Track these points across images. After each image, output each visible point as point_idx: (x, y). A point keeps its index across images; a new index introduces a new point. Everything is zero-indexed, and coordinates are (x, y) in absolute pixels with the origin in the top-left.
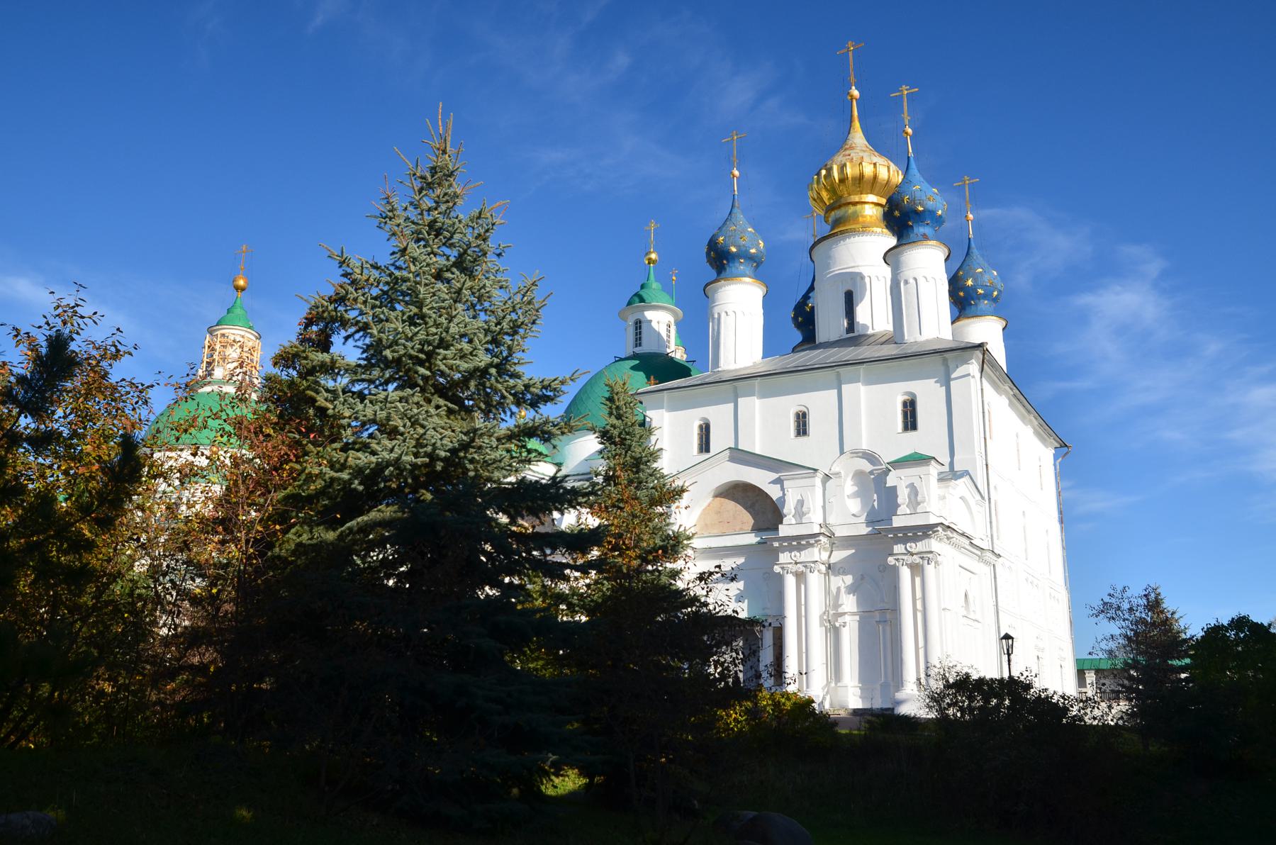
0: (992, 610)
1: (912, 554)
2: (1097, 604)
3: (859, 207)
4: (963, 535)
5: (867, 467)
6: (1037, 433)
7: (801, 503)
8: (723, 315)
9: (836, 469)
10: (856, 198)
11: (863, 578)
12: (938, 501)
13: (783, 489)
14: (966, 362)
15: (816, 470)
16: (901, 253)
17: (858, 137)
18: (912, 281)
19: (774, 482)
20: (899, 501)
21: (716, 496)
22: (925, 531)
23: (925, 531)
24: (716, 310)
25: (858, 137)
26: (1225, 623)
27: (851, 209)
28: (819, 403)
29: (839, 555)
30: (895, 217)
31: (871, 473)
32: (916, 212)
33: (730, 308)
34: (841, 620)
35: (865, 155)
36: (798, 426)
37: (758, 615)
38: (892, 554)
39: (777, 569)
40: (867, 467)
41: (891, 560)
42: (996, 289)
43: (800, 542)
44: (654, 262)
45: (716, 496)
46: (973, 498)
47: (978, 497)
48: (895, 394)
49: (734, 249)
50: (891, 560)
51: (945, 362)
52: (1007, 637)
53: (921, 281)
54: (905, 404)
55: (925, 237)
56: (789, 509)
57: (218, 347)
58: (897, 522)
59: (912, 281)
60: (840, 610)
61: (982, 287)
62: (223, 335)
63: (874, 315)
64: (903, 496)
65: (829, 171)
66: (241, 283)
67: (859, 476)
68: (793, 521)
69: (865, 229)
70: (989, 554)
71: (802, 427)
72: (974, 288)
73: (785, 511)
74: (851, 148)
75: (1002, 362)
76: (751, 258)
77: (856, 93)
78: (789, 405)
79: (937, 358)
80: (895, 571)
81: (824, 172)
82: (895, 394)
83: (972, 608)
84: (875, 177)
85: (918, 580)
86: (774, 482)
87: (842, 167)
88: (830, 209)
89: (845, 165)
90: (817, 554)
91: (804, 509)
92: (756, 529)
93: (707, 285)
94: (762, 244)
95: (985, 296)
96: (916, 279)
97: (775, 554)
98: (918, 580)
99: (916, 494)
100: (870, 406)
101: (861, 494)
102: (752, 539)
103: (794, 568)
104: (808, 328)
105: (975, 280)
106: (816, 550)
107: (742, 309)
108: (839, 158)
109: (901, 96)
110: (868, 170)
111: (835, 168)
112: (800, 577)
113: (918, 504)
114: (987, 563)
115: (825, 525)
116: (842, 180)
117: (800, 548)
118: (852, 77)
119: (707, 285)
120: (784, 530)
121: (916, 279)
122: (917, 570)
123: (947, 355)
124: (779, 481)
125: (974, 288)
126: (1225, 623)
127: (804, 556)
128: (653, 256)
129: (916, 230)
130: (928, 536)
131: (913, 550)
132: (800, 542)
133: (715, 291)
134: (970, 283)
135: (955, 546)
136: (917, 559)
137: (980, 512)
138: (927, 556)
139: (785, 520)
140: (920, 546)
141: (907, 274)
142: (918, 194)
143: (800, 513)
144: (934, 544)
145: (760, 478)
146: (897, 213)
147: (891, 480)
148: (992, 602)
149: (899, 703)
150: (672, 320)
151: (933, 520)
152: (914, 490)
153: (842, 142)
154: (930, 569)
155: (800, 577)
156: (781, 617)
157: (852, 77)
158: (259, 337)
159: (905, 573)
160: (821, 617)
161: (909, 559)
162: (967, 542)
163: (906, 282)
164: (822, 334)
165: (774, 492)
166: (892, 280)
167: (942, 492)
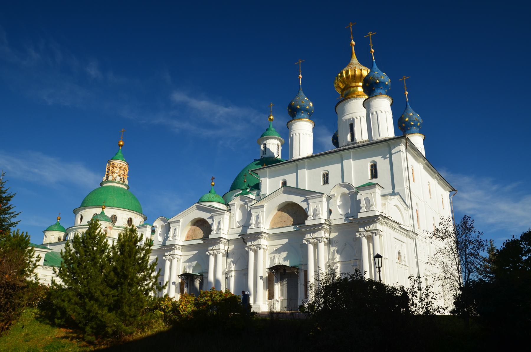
0: (415, 260)
1: (367, 231)
2: (432, 230)
3: (355, 88)
4: (394, 221)
5: (347, 191)
6: (425, 168)
7: (315, 210)
8: (294, 135)
9: (332, 193)
10: (354, 84)
11: (345, 245)
12: (378, 203)
13: (308, 204)
14: (398, 145)
15: (322, 194)
16: (371, 101)
17: (355, 60)
18: (375, 113)
19: (303, 201)
20: (361, 205)
21: (279, 210)
22: (373, 219)
23: (373, 219)
24: (292, 133)
25: (355, 60)
26: (519, 238)
27: (352, 89)
28: (334, 170)
29: (333, 235)
30: (367, 86)
31: (349, 194)
32: (376, 83)
33: (297, 132)
34: (335, 266)
35: (357, 66)
36: (324, 179)
37: (295, 264)
38: (358, 232)
39: (304, 242)
40: (347, 191)
41: (357, 235)
42: (419, 122)
43: (317, 227)
44: (272, 120)
45: (279, 210)
46: (402, 206)
47: (405, 206)
48: (367, 163)
49: (298, 107)
50: (357, 235)
51: (389, 146)
52: (378, 256)
53: (379, 113)
54: (372, 166)
55: (381, 94)
56: (310, 212)
57: (111, 168)
58: (360, 215)
59: (375, 113)
60: (335, 261)
61: (413, 121)
62: (113, 164)
63: (361, 135)
64: (363, 204)
65: (342, 74)
66: (121, 143)
67: (343, 195)
68: (312, 218)
69: (358, 96)
70: (411, 233)
71: (326, 180)
72: (409, 122)
73: (308, 214)
74: (352, 64)
75: (422, 151)
76: (306, 111)
77: (353, 43)
78: (320, 171)
79: (384, 143)
80: (359, 240)
81: (339, 74)
82: (367, 163)
83: (403, 259)
84: (361, 75)
85: (371, 245)
86: (303, 201)
87: (347, 72)
88: (343, 90)
89: (348, 71)
90: (323, 234)
91: (317, 212)
92: (294, 224)
93: (288, 123)
94: (311, 104)
95: (414, 125)
96: (376, 112)
97: (304, 234)
98: (371, 245)
99: (369, 202)
100: (356, 170)
101: (344, 206)
102: (291, 229)
103: (312, 241)
104: (334, 143)
105: (409, 118)
106: (322, 232)
107: (304, 132)
108: (346, 68)
109: (369, 37)
110: (358, 72)
111: (344, 72)
112: (316, 246)
113: (370, 206)
114: (411, 238)
115: (328, 219)
116: (348, 77)
117: (314, 232)
118: (352, 36)
119: (288, 123)
120: (308, 223)
121: (376, 112)
122: (370, 239)
123: (390, 142)
124: (306, 201)
125: (409, 122)
126: (519, 238)
127: (317, 235)
128: (272, 117)
129: (376, 91)
130: (375, 222)
131: (368, 229)
132: (317, 227)
133: (292, 125)
134: (407, 120)
135: (391, 227)
136: (370, 233)
137: (407, 214)
138: (375, 232)
139: (308, 218)
140: (371, 227)
141: (373, 110)
142: (376, 75)
143: (315, 214)
144: (378, 226)
145: (297, 199)
146: (368, 85)
147: (359, 197)
148: (414, 257)
149: (61, 253)
150: (280, 144)
151: (377, 213)
152: (368, 201)
153: (347, 62)
154: (376, 238)
155: (316, 246)
156: (306, 265)
157: (352, 36)
158: (128, 165)
159: (365, 241)
160: (326, 265)
161: (366, 234)
162: (398, 226)
163: (372, 114)
164: (342, 143)
165: (304, 206)
166: (367, 114)
167: (383, 202)
